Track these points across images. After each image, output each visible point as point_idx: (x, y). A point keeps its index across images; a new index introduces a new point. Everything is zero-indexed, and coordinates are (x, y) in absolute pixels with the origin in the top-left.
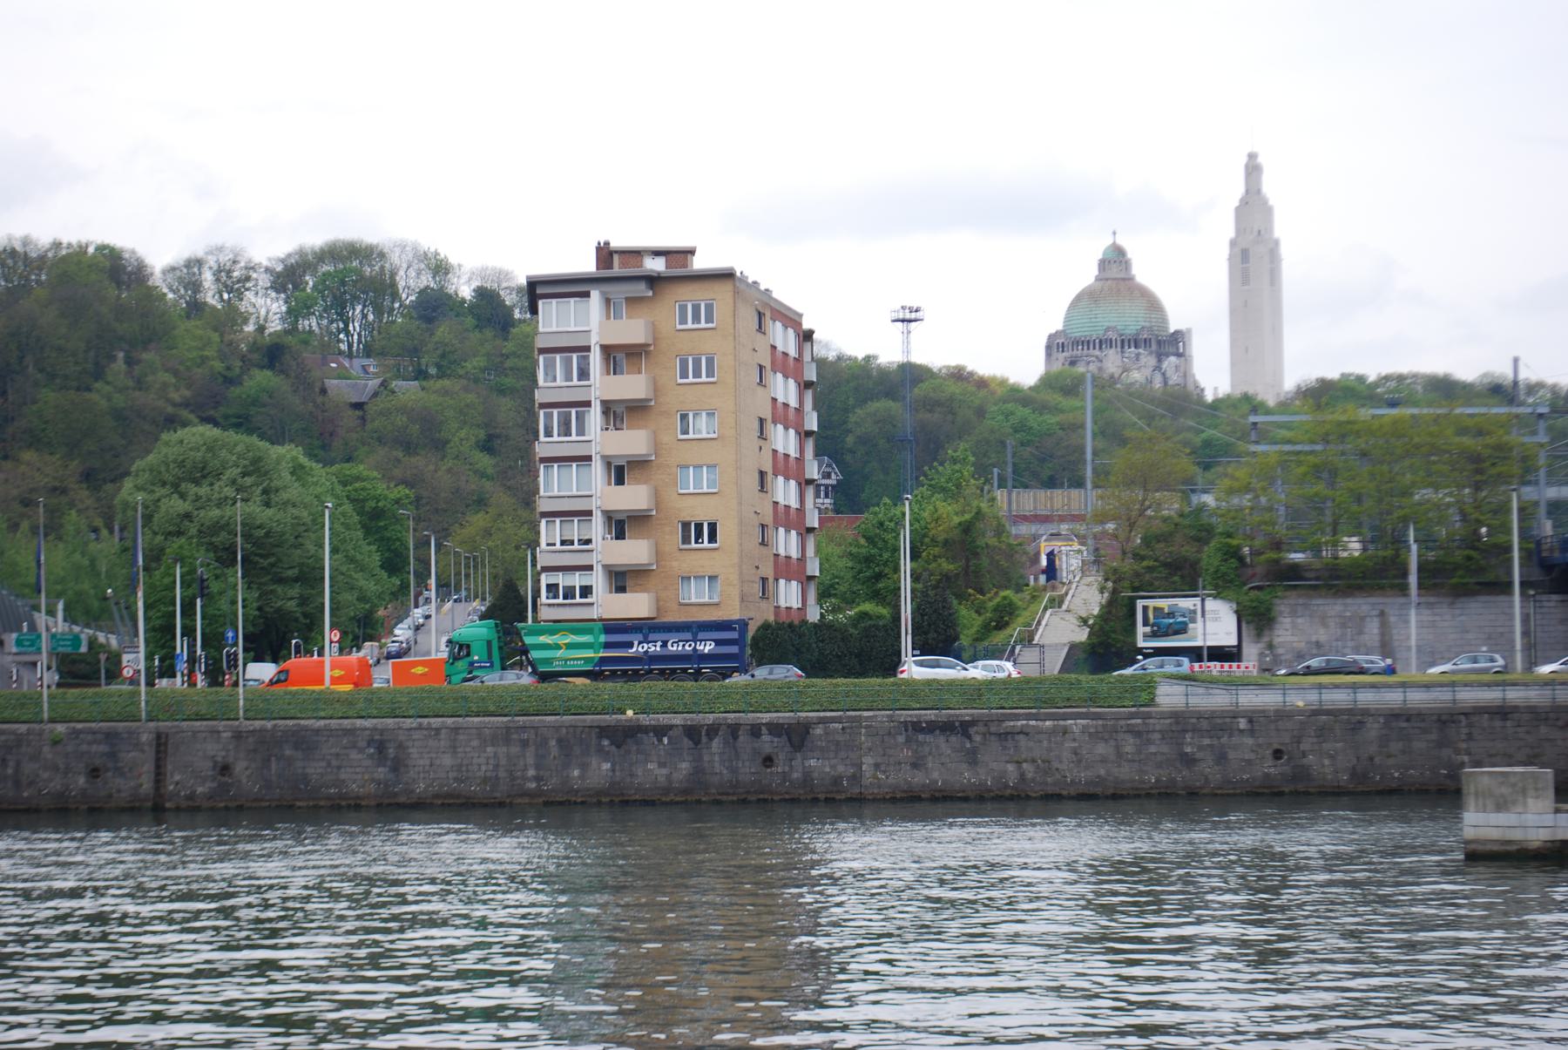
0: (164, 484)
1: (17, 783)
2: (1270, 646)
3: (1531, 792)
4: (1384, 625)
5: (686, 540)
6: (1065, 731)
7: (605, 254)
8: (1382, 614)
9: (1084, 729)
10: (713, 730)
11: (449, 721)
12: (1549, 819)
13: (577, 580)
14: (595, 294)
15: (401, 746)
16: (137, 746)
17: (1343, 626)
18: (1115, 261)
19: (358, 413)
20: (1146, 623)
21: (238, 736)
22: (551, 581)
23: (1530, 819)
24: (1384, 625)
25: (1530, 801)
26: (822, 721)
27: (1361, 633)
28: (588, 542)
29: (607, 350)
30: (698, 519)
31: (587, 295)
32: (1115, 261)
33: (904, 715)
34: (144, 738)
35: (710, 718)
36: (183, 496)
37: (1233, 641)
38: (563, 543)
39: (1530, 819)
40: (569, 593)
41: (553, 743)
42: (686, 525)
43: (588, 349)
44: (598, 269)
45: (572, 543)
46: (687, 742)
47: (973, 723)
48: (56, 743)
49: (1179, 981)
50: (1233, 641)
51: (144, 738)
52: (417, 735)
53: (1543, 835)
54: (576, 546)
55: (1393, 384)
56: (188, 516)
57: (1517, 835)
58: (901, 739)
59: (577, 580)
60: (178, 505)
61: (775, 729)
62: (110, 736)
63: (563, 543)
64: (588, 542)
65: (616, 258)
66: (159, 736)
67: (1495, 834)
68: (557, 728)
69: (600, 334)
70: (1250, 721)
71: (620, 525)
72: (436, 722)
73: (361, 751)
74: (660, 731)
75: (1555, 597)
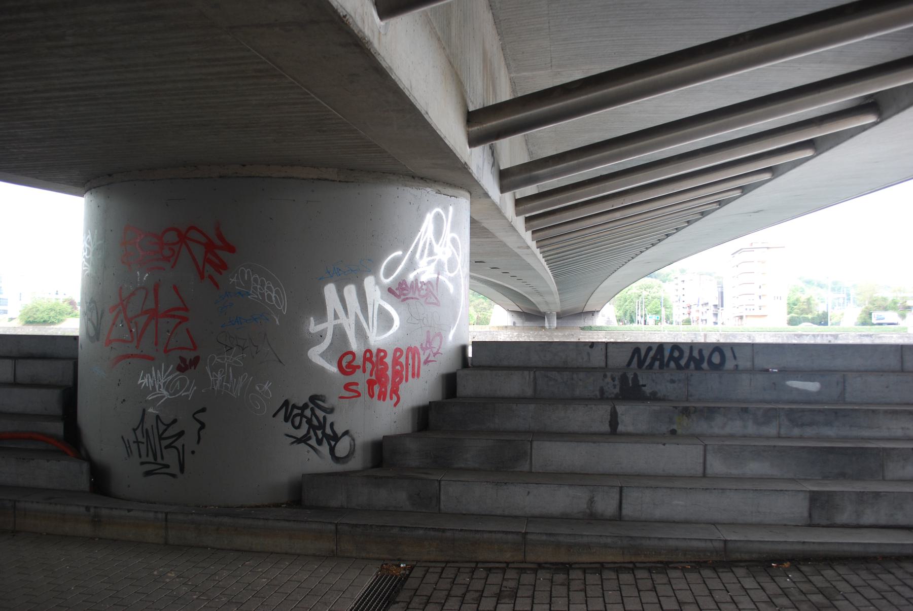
1: (552, 581)
6: (892, 337)
10: (818, 335)
13: (752, 307)
15: (754, 337)
16: (701, 336)
18: (327, 328)
19: (762, 297)
20: (875, 317)
21: (721, 334)
32: (327, 328)
33: (858, 333)
35: (817, 333)
41: (785, 337)
46: (813, 338)
47: (872, 335)
48: (684, 335)
49: (572, 254)
52: (757, 335)
58: (858, 337)
59: (752, 307)
61: (831, 335)
62: (695, 334)
66: (704, 334)
68: (786, 334)
73: (746, 338)
74: (807, 335)
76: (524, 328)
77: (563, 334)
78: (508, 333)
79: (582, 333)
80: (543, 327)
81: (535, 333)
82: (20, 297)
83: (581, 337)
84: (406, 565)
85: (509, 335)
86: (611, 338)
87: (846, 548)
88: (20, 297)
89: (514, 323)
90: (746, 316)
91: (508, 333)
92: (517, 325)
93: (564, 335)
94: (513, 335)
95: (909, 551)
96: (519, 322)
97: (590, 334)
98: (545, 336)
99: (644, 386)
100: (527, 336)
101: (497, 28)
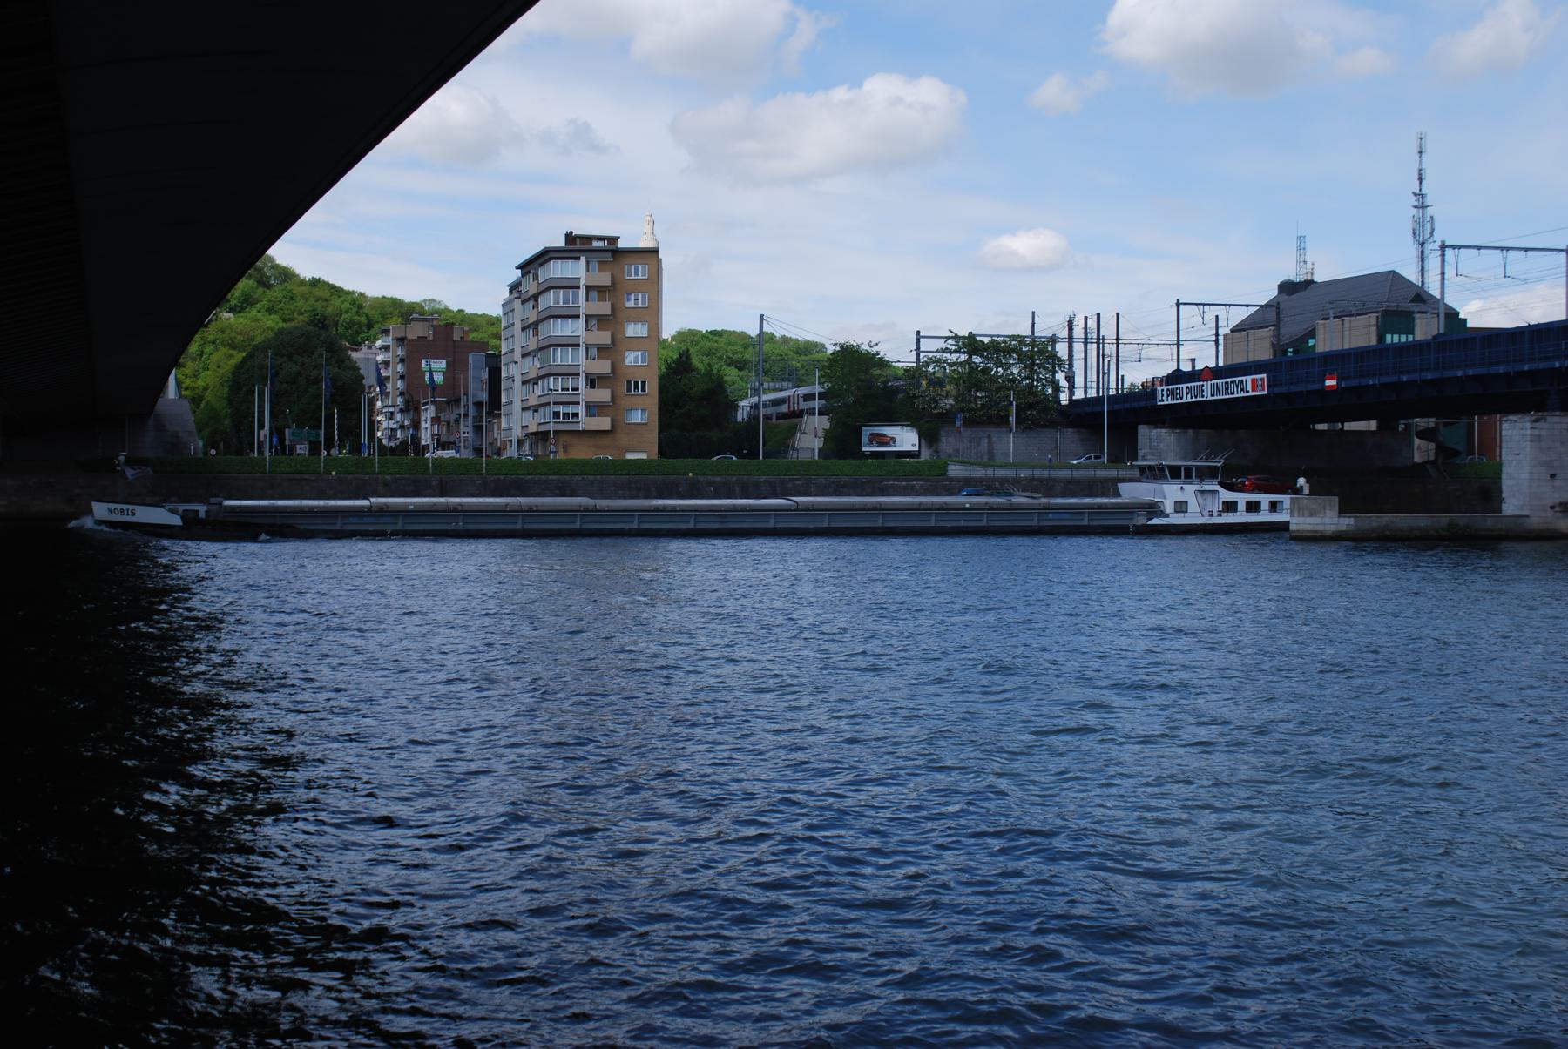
0: (282, 356)
2: (937, 451)
3: (1328, 507)
4: (990, 442)
5: (629, 390)
7: (570, 238)
8: (989, 436)
9: (922, 485)
11: (598, 477)
12: (1336, 520)
13: (570, 409)
14: (583, 259)
17: (971, 442)
22: (575, 411)
23: (1327, 520)
24: (990, 442)
25: (1328, 512)
26: (792, 480)
27: (979, 445)
28: (577, 389)
29: (588, 288)
30: (636, 379)
31: (579, 258)
34: (434, 483)
36: (296, 363)
37: (916, 448)
38: (573, 390)
39: (1327, 520)
40: (566, 415)
41: (653, 489)
42: (629, 383)
43: (578, 287)
44: (566, 244)
45: (568, 390)
50: (916, 448)
51: (434, 483)
53: (1333, 528)
54: (570, 392)
55: (326, 294)
56: (299, 373)
57: (1321, 528)
59: (570, 409)
60: (294, 368)
63: (563, 390)
64: (577, 389)
65: (578, 241)
66: (441, 481)
67: (1309, 528)
69: (586, 279)
70: (1001, 484)
71: (592, 382)
72: (591, 478)
75: (1070, 430)
84: (454, 341)
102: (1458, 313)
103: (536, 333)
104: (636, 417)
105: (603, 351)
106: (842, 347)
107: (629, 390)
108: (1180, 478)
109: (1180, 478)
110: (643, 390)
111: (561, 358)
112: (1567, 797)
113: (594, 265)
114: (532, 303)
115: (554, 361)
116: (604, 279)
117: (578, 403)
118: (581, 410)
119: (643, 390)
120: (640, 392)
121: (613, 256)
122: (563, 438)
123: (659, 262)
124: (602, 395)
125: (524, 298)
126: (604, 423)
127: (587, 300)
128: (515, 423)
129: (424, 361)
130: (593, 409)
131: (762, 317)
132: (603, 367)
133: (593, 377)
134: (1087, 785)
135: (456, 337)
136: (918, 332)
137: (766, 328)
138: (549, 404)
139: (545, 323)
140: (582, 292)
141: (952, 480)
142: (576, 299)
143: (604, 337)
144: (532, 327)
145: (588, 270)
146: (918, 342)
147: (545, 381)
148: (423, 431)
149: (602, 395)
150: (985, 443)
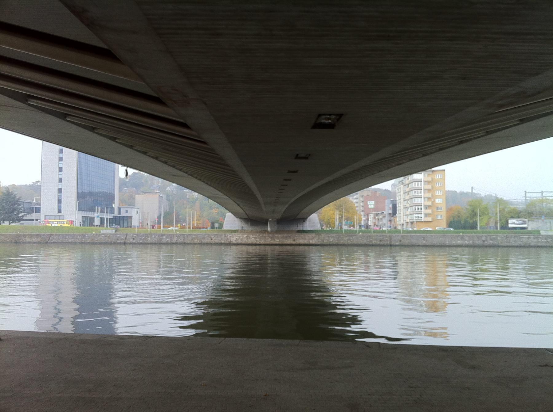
14: (423, 173)
42: (437, 208)
71: (426, 207)
76: (251, 232)
77: (282, 236)
78: (239, 235)
79: (297, 235)
80: (266, 231)
81: (260, 235)
82: (60, 201)
83: (296, 238)
84: (377, 196)
85: (240, 237)
86: (532, 298)
87: (223, 196)
88: (60, 201)
89: (242, 227)
90: (416, 222)
91: (239, 235)
92: (244, 229)
93: (283, 237)
94: (243, 236)
95: (552, 282)
96: (246, 227)
97: (302, 236)
98: (268, 238)
99: (53, 310)
100: (254, 237)
101: (225, 194)
102: (456, 192)
103: (408, 194)
104: (439, 218)
105: (429, 199)
106: (114, 208)
107: (437, 210)
108: (40, 207)
109: (40, 207)
110: (441, 209)
111: (416, 201)
112: (552, 304)
113: (426, 175)
114: (407, 186)
115: (415, 202)
116: (429, 179)
117: (422, 214)
118: (423, 216)
119: (441, 209)
120: (440, 210)
121: (432, 173)
122: (418, 223)
123: (445, 173)
124: (429, 211)
125: (404, 184)
126: (430, 219)
127: (424, 185)
128: (401, 219)
129: (368, 202)
130: (426, 215)
131: (472, 188)
132: (429, 203)
133: (427, 206)
134: (394, 285)
135: (377, 195)
136: (525, 191)
137: (474, 191)
138: (414, 214)
139: (411, 192)
140: (423, 183)
141: (542, 236)
142: (421, 184)
143: (429, 195)
144: (407, 193)
145: (424, 177)
146: (525, 194)
147: (412, 207)
148: (369, 221)
149: (429, 211)
150: (548, 224)
